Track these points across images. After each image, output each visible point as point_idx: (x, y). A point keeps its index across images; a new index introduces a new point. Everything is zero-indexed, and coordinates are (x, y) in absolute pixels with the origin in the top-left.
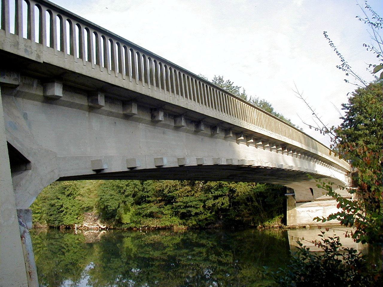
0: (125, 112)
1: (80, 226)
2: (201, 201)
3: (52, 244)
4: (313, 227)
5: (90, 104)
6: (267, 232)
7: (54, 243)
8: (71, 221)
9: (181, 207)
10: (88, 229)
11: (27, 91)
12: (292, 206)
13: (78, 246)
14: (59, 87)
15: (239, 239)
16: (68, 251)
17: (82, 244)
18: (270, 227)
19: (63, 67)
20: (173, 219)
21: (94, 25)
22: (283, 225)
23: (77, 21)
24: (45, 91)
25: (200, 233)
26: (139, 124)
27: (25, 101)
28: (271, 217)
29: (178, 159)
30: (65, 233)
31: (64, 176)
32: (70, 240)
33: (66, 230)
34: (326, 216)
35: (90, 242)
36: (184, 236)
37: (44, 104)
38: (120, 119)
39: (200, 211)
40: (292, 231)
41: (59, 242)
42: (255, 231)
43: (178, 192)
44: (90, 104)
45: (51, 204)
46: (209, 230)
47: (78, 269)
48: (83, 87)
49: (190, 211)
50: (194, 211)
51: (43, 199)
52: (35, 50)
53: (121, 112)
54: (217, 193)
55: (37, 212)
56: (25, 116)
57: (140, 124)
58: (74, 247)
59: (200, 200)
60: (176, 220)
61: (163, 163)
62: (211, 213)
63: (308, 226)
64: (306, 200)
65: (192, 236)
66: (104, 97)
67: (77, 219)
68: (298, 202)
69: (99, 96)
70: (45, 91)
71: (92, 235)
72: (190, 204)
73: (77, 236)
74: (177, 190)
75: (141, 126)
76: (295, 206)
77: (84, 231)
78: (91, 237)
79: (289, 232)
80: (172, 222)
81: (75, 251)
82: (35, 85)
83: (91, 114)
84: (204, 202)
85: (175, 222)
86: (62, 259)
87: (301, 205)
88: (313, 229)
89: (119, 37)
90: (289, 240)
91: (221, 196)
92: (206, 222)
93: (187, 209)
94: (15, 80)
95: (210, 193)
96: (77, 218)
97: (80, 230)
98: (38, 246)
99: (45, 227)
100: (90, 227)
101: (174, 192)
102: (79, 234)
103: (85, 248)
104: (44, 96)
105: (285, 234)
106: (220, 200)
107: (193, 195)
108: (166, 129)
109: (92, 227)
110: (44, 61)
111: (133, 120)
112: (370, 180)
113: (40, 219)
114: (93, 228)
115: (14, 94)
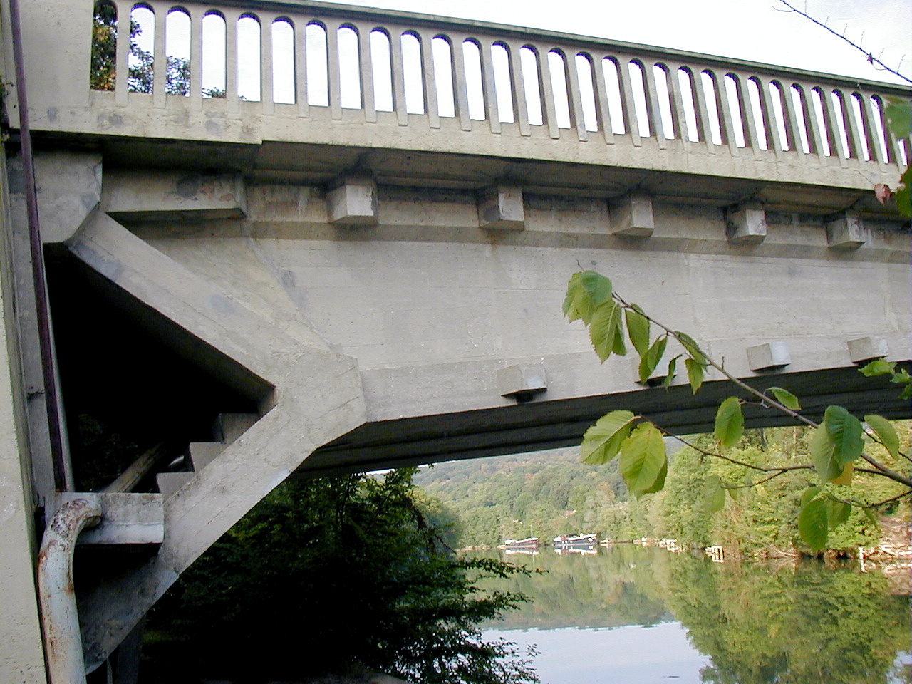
0: (616, 230)
1: (872, 551)
3: (805, 597)
5: (484, 223)
7: (811, 594)
8: (847, 539)
10: (893, 560)
11: (278, 218)
13: (870, 603)
14: (360, 192)
16: (847, 615)
17: (880, 599)
19: (325, 142)
21: (426, 18)
23: (438, 28)
24: (829, 237)
26: (687, 258)
27: (284, 242)
29: (850, 344)
30: (837, 570)
31: (401, 417)
32: (851, 589)
33: (840, 562)
35: (902, 593)
37: (344, 244)
38: (608, 251)
41: (821, 591)
44: (484, 223)
45: (796, 500)
47: (874, 663)
48: (454, 184)
51: (780, 487)
52: (238, 118)
53: (607, 231)
55: (767, 519)
56: (288, 280)
57: (691, 256)
58: (860, 606)
61: (772, 360)
66: (520, 197)
67: (863, 533)
69: (501, 196)
70: (330, 212)
71: (905, 575)
73: (866, 579)
75: (696, 262)
77: (882, 565)
78: (903, 581)
81: (865, 615)
82: (302, 203)
83: (500, 248)
86: (831, 635)
89: (523, 30)
94: (227, 197)
96: (863, 531)
97: (872, 561)
98: (776, 600)
99: (790, 555)
100: (897, 553)
102: (871, 573)
103: (889, 608)
104: (330, 223)
108: (797, 261)
109: (903, 553)
110: (266, 139)
111: (380, 238)
113: (775, 538)
114: (905, 557)
115: (248, 232)
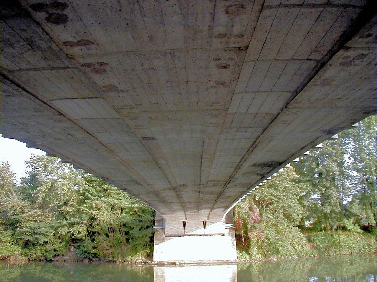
2: (52, 227)
4: (182, 264)
6: (129, 268)
9: (27, 234)
12: (160, 240)
15: (93, 276)
18: (133, 262)
20: (13, 248)
22: (57, 270)
25: (44, 266)
28: (135, 250)
34: (39, 34)
36: (25, 269)
39: (50, 240)
40: (159, 268)
42: (113, 266)
43: (25, 215)
46: (56, 262)
49: (37, 238)
50: (42, 239)
54: (73, 220)
59: (50, 227)
60: (18, 249)
62: (61, 242)
63: (177, 263)
64: (176, 234)
65: (35, 269)
68: (167, 237)
72: (39, 230)
74: (25, 213)
76: (163, 240)
79: (157, 270)
80: (11, 251)
84: (56, 229)
85: (15, 251)
87: (171, 239)
88: (183, 266)
90: (155, 278)
91: (78, 223)
92: (55, 253)
93: (34, 236)
95: (65, 219)
101: (21, 215)
105: (150, 272)
106: (76, 228)
107: (42, 221)
112: (247, 216)
